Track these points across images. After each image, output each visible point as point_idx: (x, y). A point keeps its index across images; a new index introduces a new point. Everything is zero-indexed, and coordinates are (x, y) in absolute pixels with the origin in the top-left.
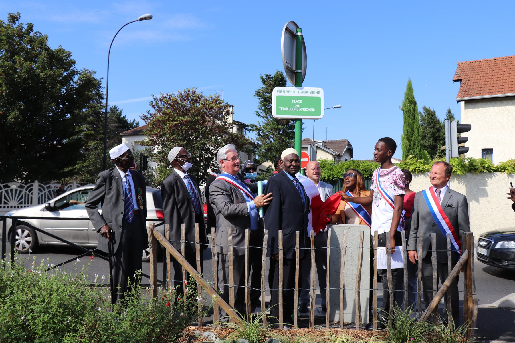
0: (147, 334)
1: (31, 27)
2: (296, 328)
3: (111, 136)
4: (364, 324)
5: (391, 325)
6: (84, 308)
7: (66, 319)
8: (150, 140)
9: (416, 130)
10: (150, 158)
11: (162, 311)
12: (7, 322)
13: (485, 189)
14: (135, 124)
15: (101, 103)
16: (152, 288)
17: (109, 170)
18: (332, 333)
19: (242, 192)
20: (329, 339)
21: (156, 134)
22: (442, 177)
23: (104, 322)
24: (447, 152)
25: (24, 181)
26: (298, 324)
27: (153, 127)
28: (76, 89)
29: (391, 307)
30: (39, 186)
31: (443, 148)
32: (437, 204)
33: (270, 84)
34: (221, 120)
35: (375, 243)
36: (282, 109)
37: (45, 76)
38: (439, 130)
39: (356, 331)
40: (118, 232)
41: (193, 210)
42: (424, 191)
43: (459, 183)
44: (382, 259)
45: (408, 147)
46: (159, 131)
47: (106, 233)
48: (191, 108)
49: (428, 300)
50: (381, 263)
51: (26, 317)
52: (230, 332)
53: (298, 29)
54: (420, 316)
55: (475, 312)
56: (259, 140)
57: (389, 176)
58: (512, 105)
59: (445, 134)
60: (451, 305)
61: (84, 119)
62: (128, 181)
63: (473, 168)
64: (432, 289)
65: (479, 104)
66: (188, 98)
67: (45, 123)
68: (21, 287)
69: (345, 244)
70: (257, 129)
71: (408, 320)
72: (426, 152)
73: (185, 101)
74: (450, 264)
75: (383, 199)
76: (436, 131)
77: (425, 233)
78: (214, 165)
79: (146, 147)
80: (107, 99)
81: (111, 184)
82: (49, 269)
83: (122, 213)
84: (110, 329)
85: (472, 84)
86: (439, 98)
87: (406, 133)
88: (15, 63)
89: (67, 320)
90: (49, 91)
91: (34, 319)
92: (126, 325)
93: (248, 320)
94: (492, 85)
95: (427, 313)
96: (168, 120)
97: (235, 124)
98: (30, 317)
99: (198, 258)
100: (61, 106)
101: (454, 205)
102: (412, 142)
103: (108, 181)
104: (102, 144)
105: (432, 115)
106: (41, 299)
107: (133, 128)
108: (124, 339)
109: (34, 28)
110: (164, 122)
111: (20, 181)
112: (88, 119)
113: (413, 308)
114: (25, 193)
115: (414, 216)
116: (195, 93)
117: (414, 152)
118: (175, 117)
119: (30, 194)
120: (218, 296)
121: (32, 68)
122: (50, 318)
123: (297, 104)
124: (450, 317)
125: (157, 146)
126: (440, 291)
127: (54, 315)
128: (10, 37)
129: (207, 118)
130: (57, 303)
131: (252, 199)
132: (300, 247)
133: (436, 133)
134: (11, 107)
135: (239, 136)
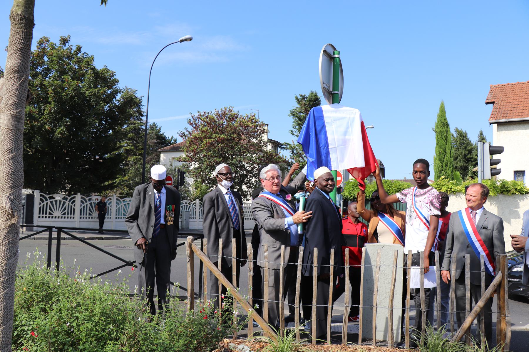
0: (185, 345)
1: (79, 49)
2: (328, 344)
3: (150, 152)
4: (396, 342)
5: (423, 343)
6: (124, 318)
7: (108, 327)
8: (187, 156)
9: (448, 151)
10: (187, 174)
11: (200, 324)
12: (54, 328)
13: (517, 211)
14: (173, 141)
15: (141, 120)
16: (189, 301)
17: (144, 184)
18: (364, 350)
19: (283, 208)
21: (193, 151)
22: (477, 199)
23: (143, 332)
24: (479, 174)
25: (67, 193)
26: (331, 340)
27: (190, 144)
28: (118, 107)
29: (424, 325)
30: (82, 198)
31: (475, 169)
32: (472, 225)
33: (305, 104)
34: (257, 138)
35: (409, 262)
37: (90, 94)
38: (470, 152)
39: (388, 349)
41: (232, 225)
42: (460, 211)
43: (491, 205)
44: (416, 279)
45: (441, 168)
46: (196, 147)
47: (141, 244)
48: (227, 127)
49: (460, 320)
50: (414, 283)
51: (71, 323)
52: (263, 346)
53: (335, 52)
54: (452, 337)
55: (509, 335)
57: (425, 196)
59: (477, 155)
60: (483, 326)
61: (125, 135)
63: (505, 190)
64: (464, 309)
65: (512, 127)
67: (89, 139)
68: (67, 295)
69: (379, 263)
70: (291, 148)
71: (440, 339)
72: (458, 173)
73: (221, 119)
74: (483, 284)
75: (418, 219)
76: (467, 152)
77: (458, 253)
78: (248, 182)
79: (183, 162)
80: (147, 116)
82: (91, 278)
84: (149, 339)
85: (504, 107)
86: (472, 121)
87: (438, 154)
88: (64, 82)
89: (109, 328)
90: (94, 108)
91: (78, 326)
92: (164, 336)
93: (281, 335)
94: (524, 108)
95: (460, 333)
96: (205, 137)
97: (270, 142)
98: (74, 324)
99: (234, 273)
101: (490, 227)
102: (444, 163)
104: (141, 159)
105: (464, 137)
106: (85, 308)
107: (171, 144)
108: (162, 349)
109: (82, 49)
111: (63, 193)
112: (129, 136)
113: (445, 328)
114: (69, 204)
115: (449, 236)
116: (231, 111)
117: (446, 173)
118: (212, 135)
119: (73, 205)
120: (254, 311)
121: (79, 86)
122: (94, 326)
124: (483, 339)
125: (193, 162)
126: (473, 311)
127: (96, 323)
128: (60, 58)
129: (243, 136)
130: (100, 311)
131: (292, 215)
132: (334, 264)
133: (468, 154)
134: (58, 123)
135: (274, 154)
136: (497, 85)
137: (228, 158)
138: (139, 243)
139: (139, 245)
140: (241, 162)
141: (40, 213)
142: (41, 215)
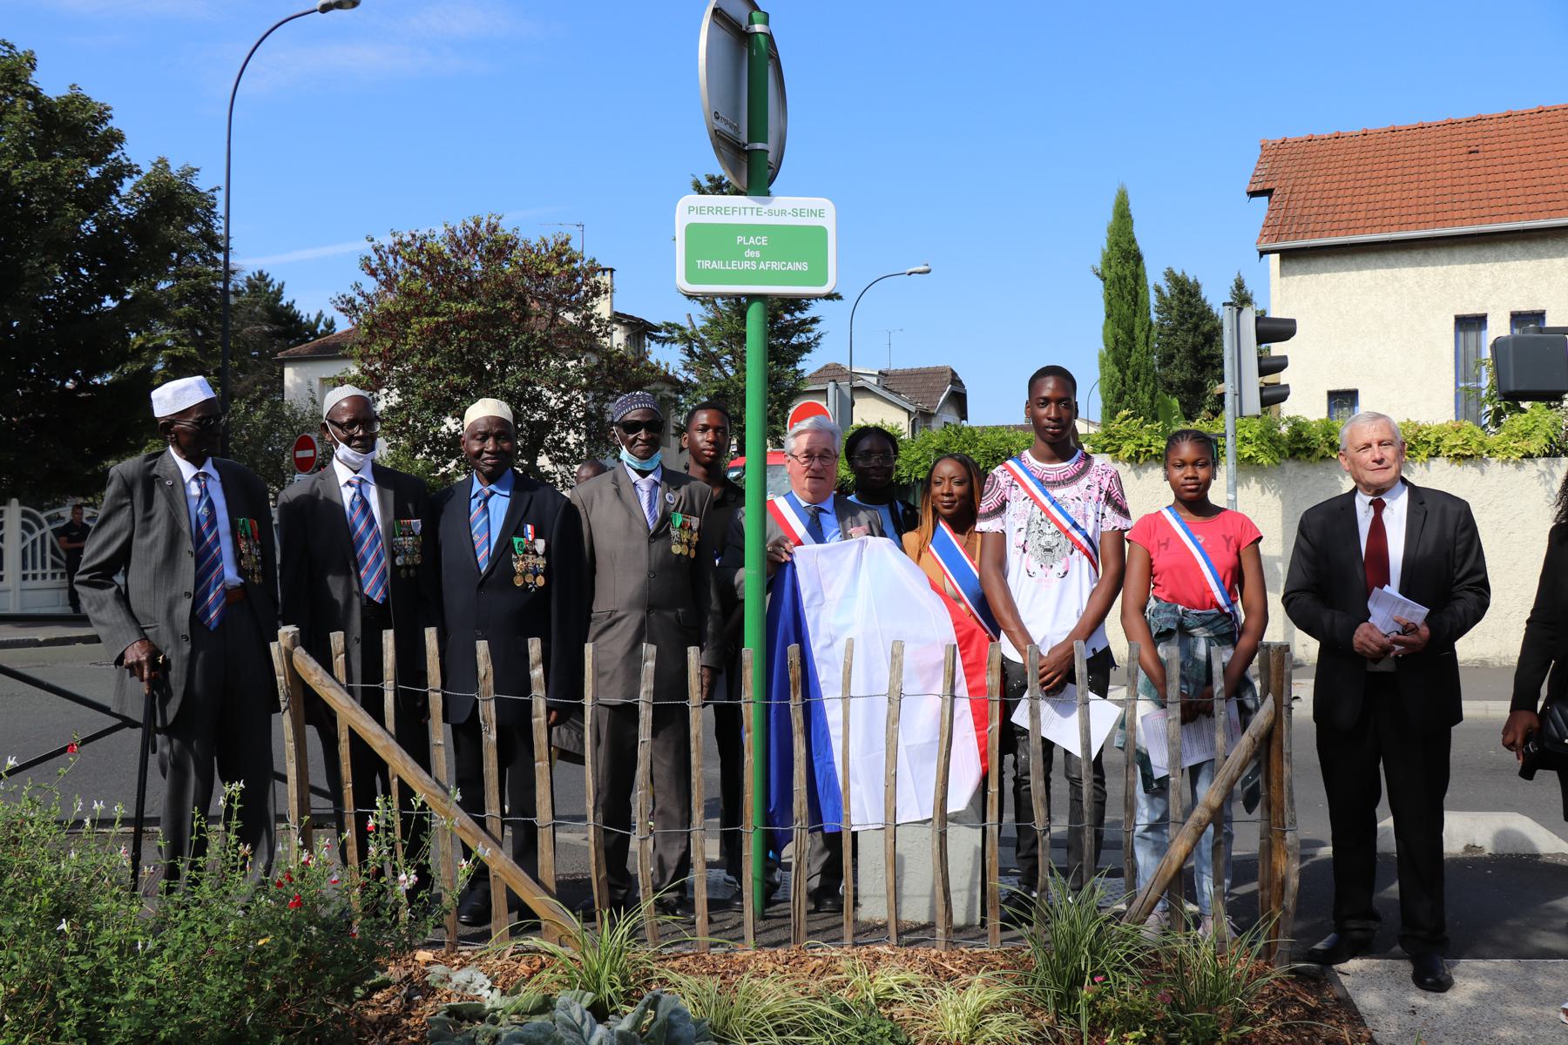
14: (322, 327)
20: (847, 981)
21: (380, 355)
24: (1228, 402)
27: (371, 333)
30: (25, 514)
31: (1219, 388)
36: (706, 264)
39: (934, 952)
40: (177, 654)
43: (1263, 492)
45: (1119, 385)
46: (389, 344)
47: (139, 664)
53: (755, 15)
56: (691, 371)
58: (1409, 265)
62: (205, 491)
66: (474, 246)
70: (686, 338)
72: (1176, 402)
76: (1200, 339)
83: (188, 594)
86: (1208, 244)
87: (1112, 345)
96: (417, 312)
97: (619, 322)
100: (84, 272)
103: (138, 492)
110: (405, 319)
117: (1135, 400)
118: (438, 303)
123: (753, 247)
133: (1203, 345)
135: (631, 357)
136: (1279, 139)
137: (491, 374)
138: (130, 658)
139: (131, 667)
140: (529, 383)
142: (30, 571)
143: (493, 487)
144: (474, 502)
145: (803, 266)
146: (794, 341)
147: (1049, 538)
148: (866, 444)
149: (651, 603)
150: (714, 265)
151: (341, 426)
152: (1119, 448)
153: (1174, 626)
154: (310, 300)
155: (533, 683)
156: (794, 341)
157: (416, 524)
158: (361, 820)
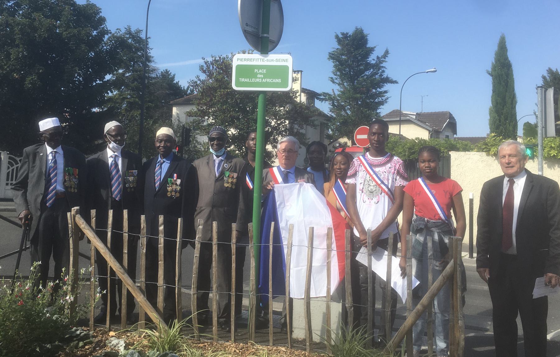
8: (199, 110)
14: (189, 91)
33: (347, 44)
36: (243, 80)
40: (36, 214)
45: (498, 122)
55: (462, 343)
79: (195, 118)
81: (34, 162)
96: (220, 87)
102: (502, 116)
103: (31, 157)
107: (187, 95)
123: (261, 74)
141: (8, 180)
143: (164, 160)
144: (157, 165)
145: (279, 81)
146: (376, 100)
147: (372, 187)
148: (313, 148)
149: (214, 205)
150: (246, 80)
151: (112, 136)
152: (490, 150)
153: (423, 227)
154: (183, 82)
155: (160, 232)
156: (376, 100)
157: (135, 172)
158: (76, 272)
